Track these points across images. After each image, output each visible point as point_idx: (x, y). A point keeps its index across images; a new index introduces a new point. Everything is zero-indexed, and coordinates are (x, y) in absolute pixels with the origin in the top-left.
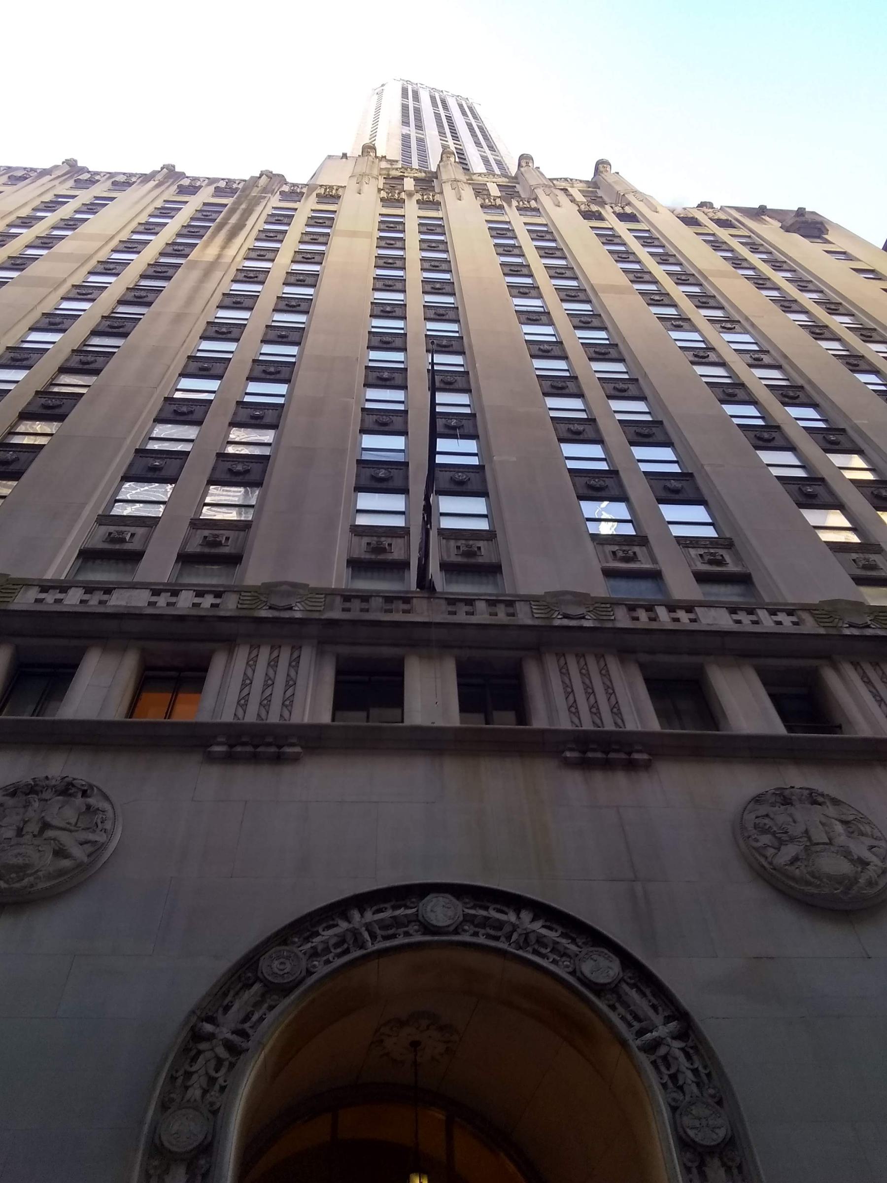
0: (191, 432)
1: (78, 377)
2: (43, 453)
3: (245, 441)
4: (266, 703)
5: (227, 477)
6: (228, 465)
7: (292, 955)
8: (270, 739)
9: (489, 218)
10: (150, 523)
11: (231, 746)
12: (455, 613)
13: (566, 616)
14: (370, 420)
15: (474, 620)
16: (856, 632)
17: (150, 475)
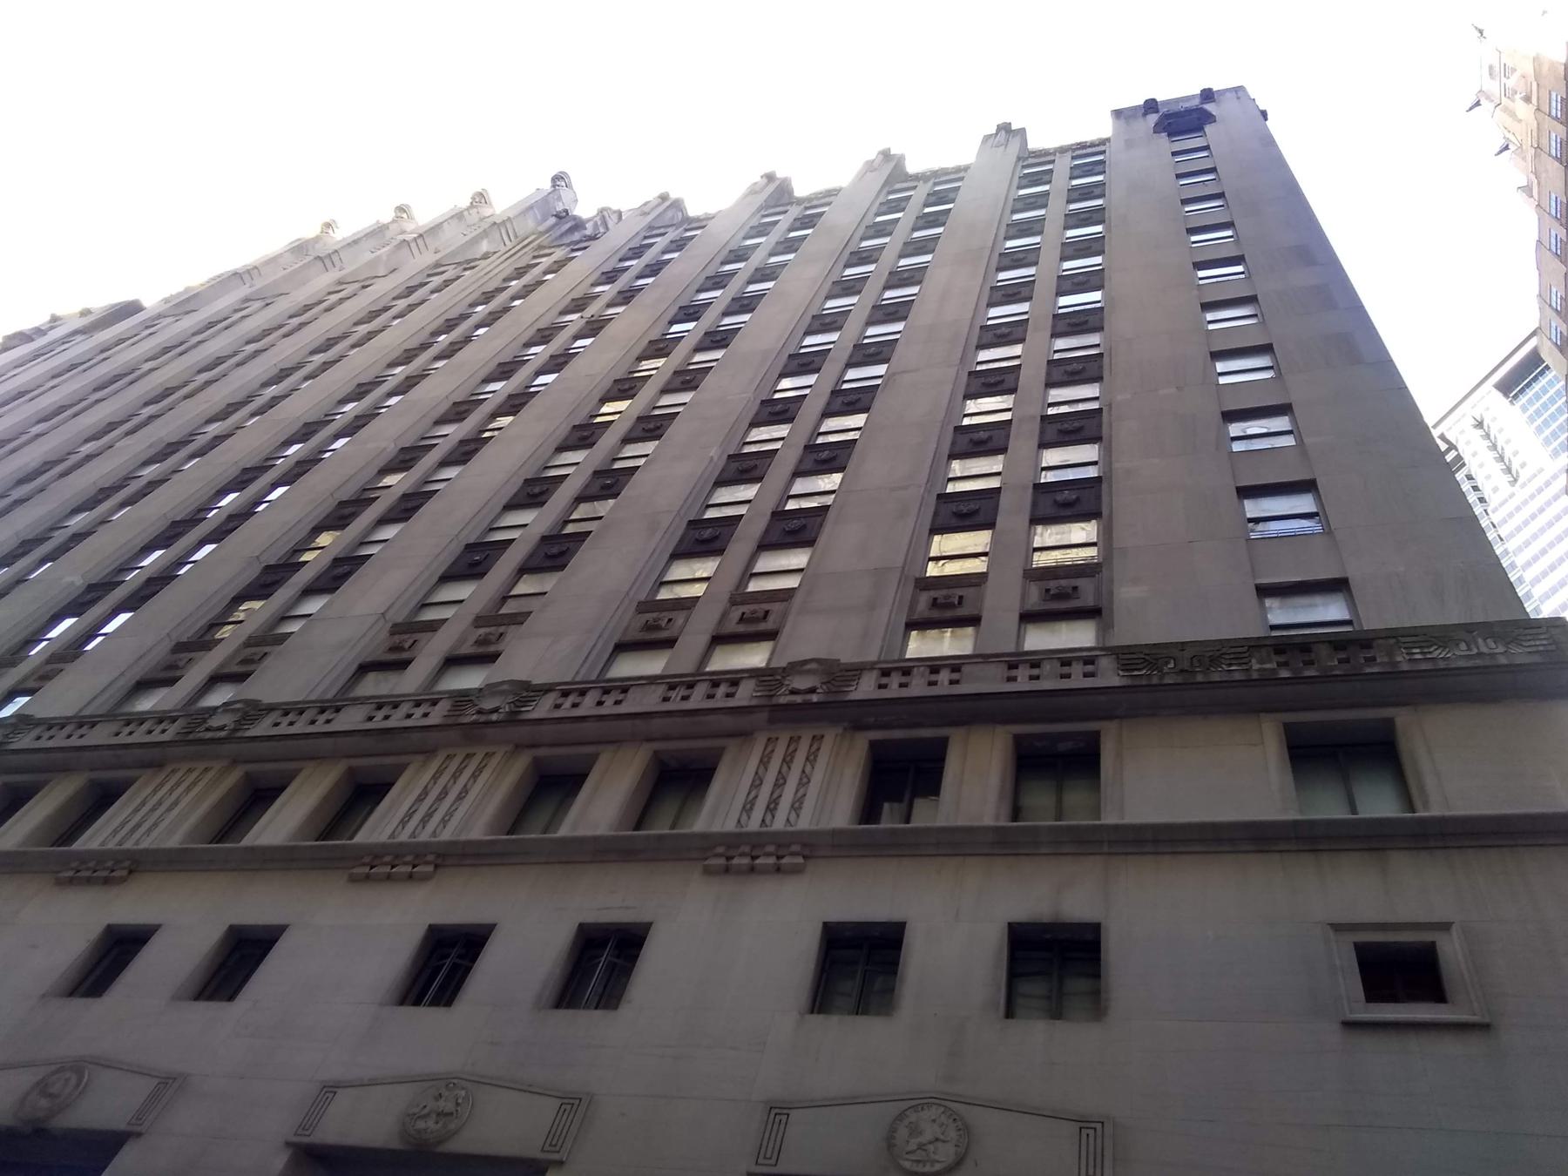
0: (995, 464)
1: (999, 398)
2: (831, 514)
3: (1069, 461)
4: (772, 807)
5: (954, 522)
6: (953, 507)
7: (913, 1117)
8: (796, 848)
9: (1178, 147)
10: (976, 580)
11: (779, 858)
12: (1068, 676)
13: (793, 692)
14: (964, 440)
15: (691, 705)
16: (798, 699)
17: (790, 539)
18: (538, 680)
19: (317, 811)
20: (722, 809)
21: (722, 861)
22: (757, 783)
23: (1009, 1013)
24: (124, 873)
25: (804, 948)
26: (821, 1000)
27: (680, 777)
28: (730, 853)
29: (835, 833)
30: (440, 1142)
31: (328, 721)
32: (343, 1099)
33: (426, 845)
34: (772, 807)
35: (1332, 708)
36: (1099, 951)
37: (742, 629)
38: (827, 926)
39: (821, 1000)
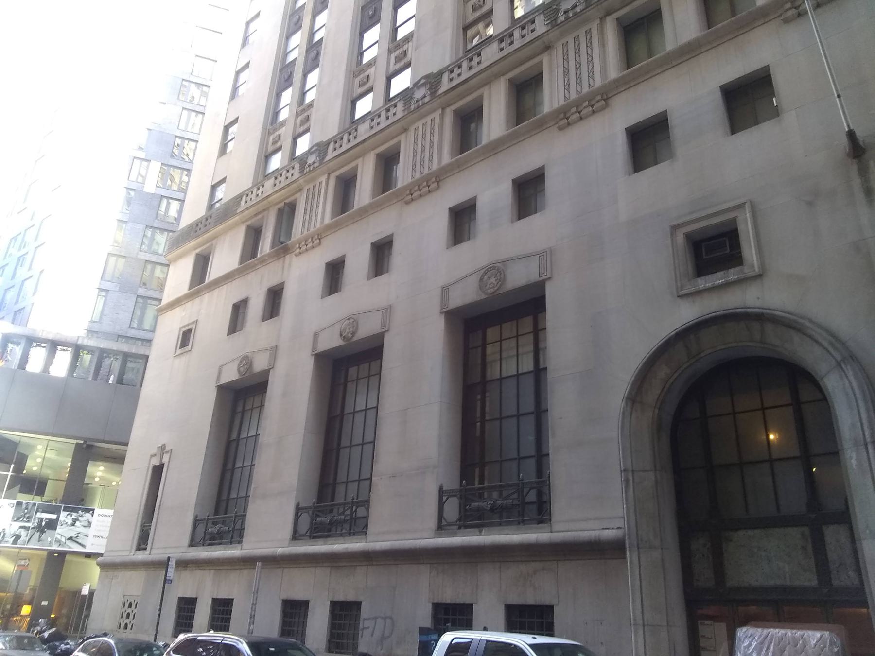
4: (579, 81)
18: (435, 70)
19: (375, 182)
20: (552, 97)
21: (794, 11)
22: (566, 72)
23: (733, 131)
24: (436, 184)
25: (621, 144)
26: (735, 125)
27: (525, 89)
28: (592, 103)
29: (616, 81)
30: (353, 334)
31: (479, 63)
32: (225, 369)
33: (429, 174)
34: (579, 81)
35: (379, 146)
36: (771, 80)
37: (398, 66)
38: (514, 181)
39: (735, 125)
